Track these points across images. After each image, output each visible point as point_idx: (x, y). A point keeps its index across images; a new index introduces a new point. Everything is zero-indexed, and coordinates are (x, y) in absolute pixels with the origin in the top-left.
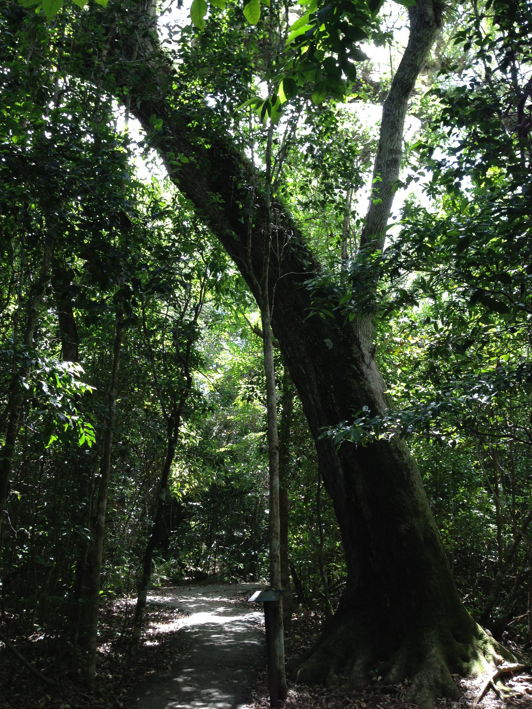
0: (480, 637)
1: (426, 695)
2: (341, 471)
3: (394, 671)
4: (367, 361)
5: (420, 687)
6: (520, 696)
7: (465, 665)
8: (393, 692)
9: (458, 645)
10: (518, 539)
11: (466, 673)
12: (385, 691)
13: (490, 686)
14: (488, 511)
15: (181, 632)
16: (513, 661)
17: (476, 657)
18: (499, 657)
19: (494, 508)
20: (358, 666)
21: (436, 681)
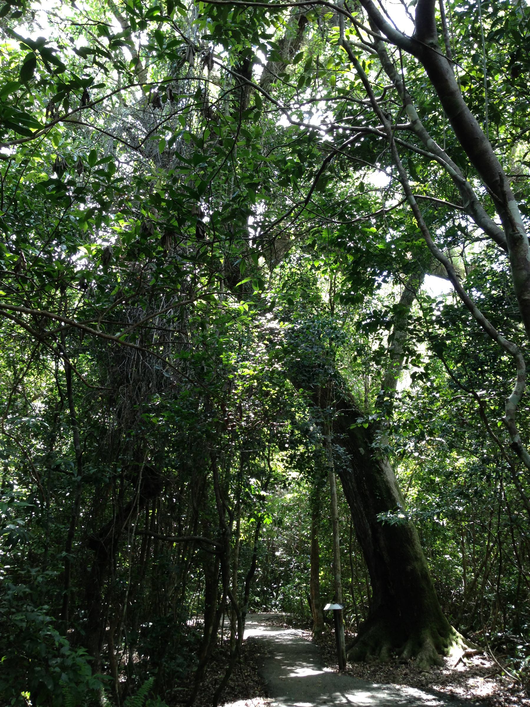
0: (454, 634)
1: (425, 664)
2: (370, 532)
3: (405, 652)
4: (385, 462)
5: (421, 660)
6: (477, 666)
7: (446, 649)
8: (406, 663)
9: (441, 638)
10: (477, 576)
11: (446, 654)
12: (401, 663)
13: (460, 660)
14: (455, 556)
15: (272, 630)
16: (473, 648)
17: (451, 644)
18: (466, 646)
19: (460, 555)
20: (384, 650)
21: (430, 657)
